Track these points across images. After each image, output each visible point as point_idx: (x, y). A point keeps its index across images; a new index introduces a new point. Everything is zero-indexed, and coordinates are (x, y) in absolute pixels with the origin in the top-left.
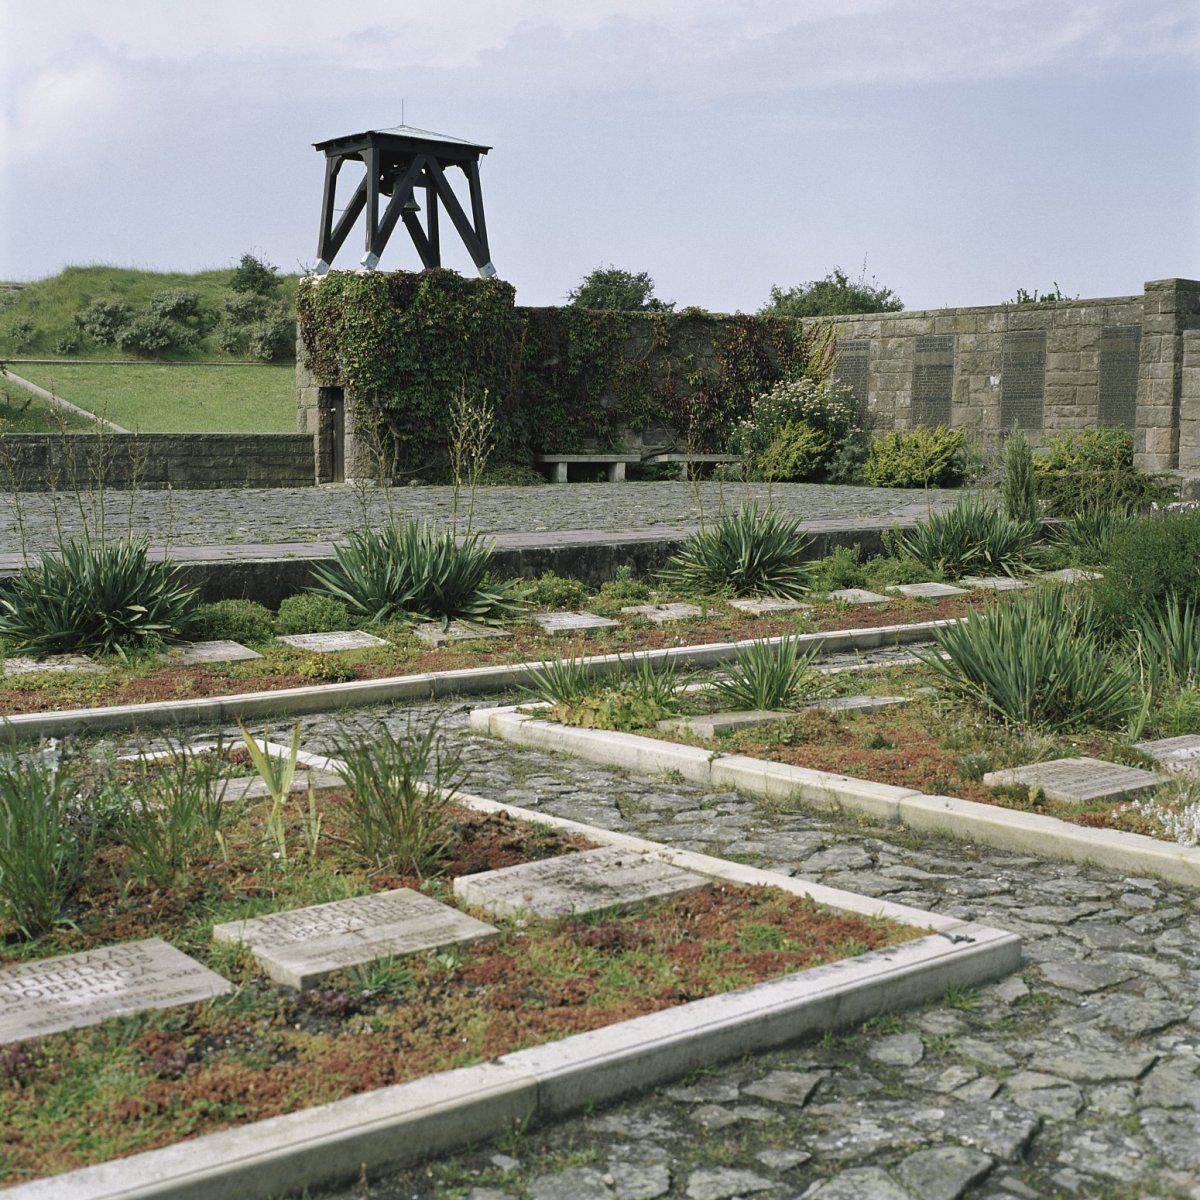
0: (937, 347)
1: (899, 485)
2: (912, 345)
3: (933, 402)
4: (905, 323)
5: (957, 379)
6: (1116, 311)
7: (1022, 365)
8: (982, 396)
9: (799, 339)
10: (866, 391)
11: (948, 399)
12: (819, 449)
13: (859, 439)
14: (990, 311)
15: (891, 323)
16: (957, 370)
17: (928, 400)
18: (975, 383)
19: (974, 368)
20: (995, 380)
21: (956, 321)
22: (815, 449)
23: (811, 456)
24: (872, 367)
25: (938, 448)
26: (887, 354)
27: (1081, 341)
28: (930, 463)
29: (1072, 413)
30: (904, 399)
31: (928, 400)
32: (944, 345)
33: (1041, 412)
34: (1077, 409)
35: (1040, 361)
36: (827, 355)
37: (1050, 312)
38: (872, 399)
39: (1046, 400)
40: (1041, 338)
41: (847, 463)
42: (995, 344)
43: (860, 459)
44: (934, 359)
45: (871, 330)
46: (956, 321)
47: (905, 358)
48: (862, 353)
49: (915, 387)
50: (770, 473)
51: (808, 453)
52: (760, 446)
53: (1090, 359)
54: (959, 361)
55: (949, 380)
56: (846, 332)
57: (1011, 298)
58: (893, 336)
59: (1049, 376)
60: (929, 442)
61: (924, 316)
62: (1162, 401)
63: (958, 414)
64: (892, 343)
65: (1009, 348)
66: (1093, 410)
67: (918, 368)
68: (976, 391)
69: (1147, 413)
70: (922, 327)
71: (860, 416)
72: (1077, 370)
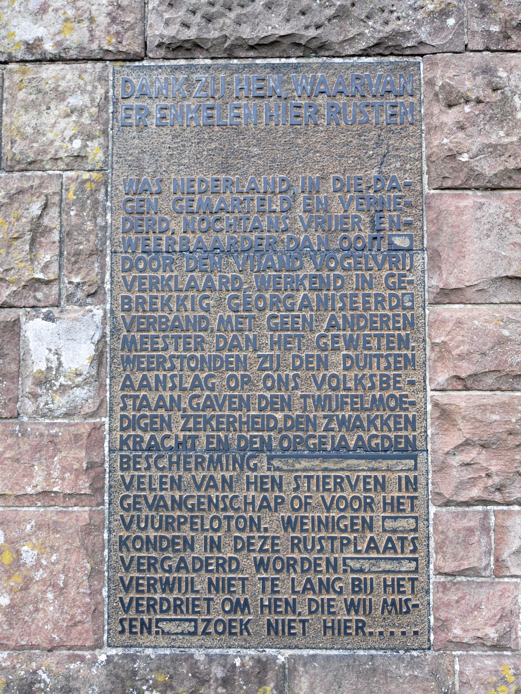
33: (410, 543)
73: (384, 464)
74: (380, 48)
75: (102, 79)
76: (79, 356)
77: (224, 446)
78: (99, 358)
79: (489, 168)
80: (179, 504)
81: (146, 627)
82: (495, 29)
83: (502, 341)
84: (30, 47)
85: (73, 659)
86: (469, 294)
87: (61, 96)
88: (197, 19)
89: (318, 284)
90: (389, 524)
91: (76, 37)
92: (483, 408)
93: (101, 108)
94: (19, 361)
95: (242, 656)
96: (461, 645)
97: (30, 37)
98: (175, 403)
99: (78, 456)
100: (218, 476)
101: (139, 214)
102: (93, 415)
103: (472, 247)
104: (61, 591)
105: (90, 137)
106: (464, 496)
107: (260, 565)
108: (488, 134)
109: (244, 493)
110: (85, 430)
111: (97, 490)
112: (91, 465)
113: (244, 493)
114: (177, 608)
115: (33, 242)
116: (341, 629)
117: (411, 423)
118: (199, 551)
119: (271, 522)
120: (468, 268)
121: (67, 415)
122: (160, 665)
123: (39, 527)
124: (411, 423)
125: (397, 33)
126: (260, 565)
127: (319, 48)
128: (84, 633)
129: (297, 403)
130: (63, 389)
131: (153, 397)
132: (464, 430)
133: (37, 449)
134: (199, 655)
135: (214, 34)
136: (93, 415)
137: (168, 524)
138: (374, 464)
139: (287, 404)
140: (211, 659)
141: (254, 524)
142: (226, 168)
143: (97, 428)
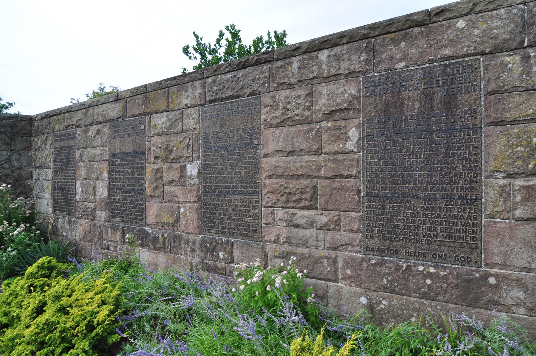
33: (258, 216)
35: (252, 140)
39: (266, 199)
46: (146, 100)
73: (252, 197)
74: (251, 94)
75: (198, 110)
76: (195, 172)
77: (221, 192)
78: (199, 173)
79: (275, 122)
80: (213, 205)
81: (208, 231)
82: (276, 85)
83: (276, 167)
84: (186, 105)
85: (196, 236)
86: (271, 155)
87: (192, 115)
88: (214, 94)
89: (239, 154)
90: (253, 211)
91: (193, 102)
92: (272, 183)
93: (198, 117)
94: (186, 173)
95: (224, 239)
96: (268, 241)
97: (186, 103)
98: (212, 183)
99: (195, 193)
100: (220, 198)
101: (206, 141)
102: (198, 185)
103: (271, 143)
104: (193, 222)
105: (197, 124)
106: (268, 205)
107: (228, 219)
108: (274, 113)
109: (225, 203)
110: (196, 188)
111: (199, 201)
112: (197, 196)
113: (225, 203)
114: (213, 227)
115: (187, 148)
116: (243, 235)
117: (258, 187)
118: (217, 216)
119: (230, 209)
120: (270, 149)
121: (194, 185)
122: (210, 239)
123: (189, 208)
124: (258, 187)
125: (253, 91)
126: (228, 219)
127: (238, 97)
128: (197, 231)
129: (235, 182)
130: (193, 179)
131: (208, 181)
132: (268, 189)
133: (189, 192)
134: (217, 238)
135: (218, 97)
136: (198, 185)
137: (211, 209)
138: (250, 197)
139: (233, 183)
140: (219, 239)
141: (227, 210)
142: (221, 128)
143: (199, 188)
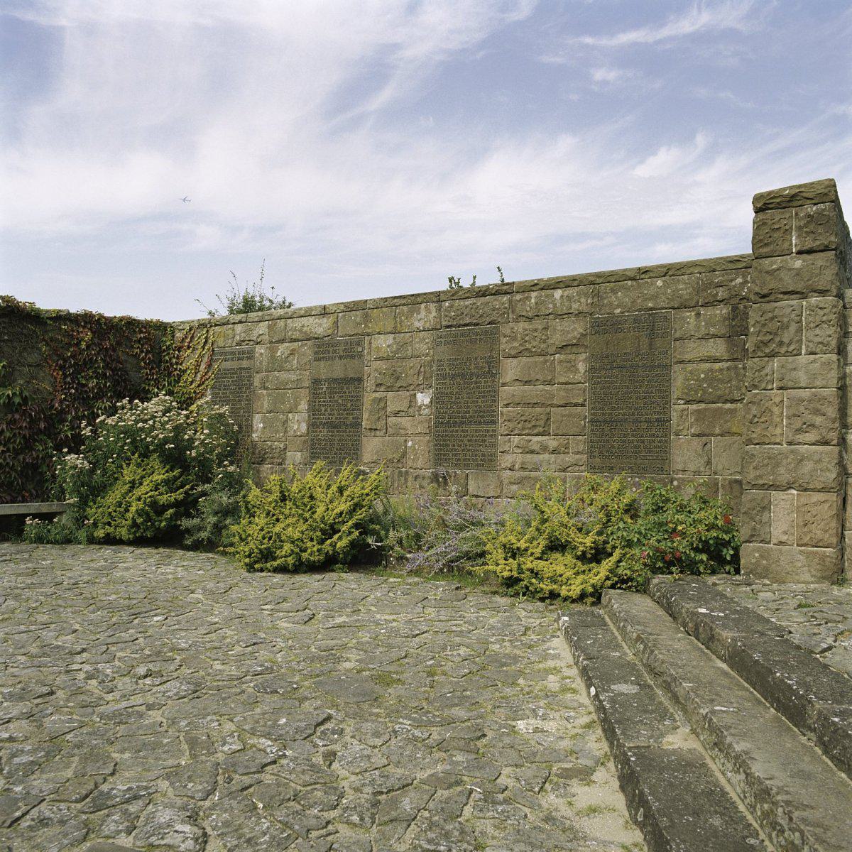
0: (342, 347)
1: (282, 570)
2: (307, 350)
3: (336, 435)
4: (298, 323)
5: (369, 397)
6: (614, 291)
7: (463, 376)
8: (405, 421)
9: (168, 348)
10: (249, 413)
11: (358, 424)
12: (173, 497)
13: (234, 484)
14: (414, 301)
15: (281, 323)
16: (369, 384)
17: (332, 426)
18: (395, 401)
19: (393, 382)
20: (423, 398)
21: (366, 318)
22: (164, 499)
23: (159, 509)
24: (257, 383)
25: (344, 506)
26: (277, 365)
27: (557, 339)
28: (332, 530)
29: (544, 449)
30: (299, 424)
31: (332, 426)
32: (351, 349)
33: (494, 445)
34: (552, 443)
35: (491, 369)
36: (203, 367)
37: (505, 298)
38: (258, 423)
39: (502, 429)
40: (492, 336)
41: (213, 519)
42: (422, 346)
43: (230, 512)
44: (338, 369)
45: (255, 333)
46: (366, 317)
47: (299, 369)
48: (245, 364)
49: (313, 409)
50: (100, 533)
51: (154, 504)
52: (92, 490)
53: (572, 368)
54: (373, 370)
55: (358, 399)
56: (226, 337)
57: (444, 286)
58: (282, 341)
59: (506, 392)
60: (329, 492)
61: (324, 312)
62: (812, 436)
63: (371, 446)
64: (282, 350)
65: (444, 352)
66: (580, 443)
67: (316, 382)
68: (396, 414)
69: (775, 461)
70: (321, 327)
71: (236, 444)
72: (550, 383)
